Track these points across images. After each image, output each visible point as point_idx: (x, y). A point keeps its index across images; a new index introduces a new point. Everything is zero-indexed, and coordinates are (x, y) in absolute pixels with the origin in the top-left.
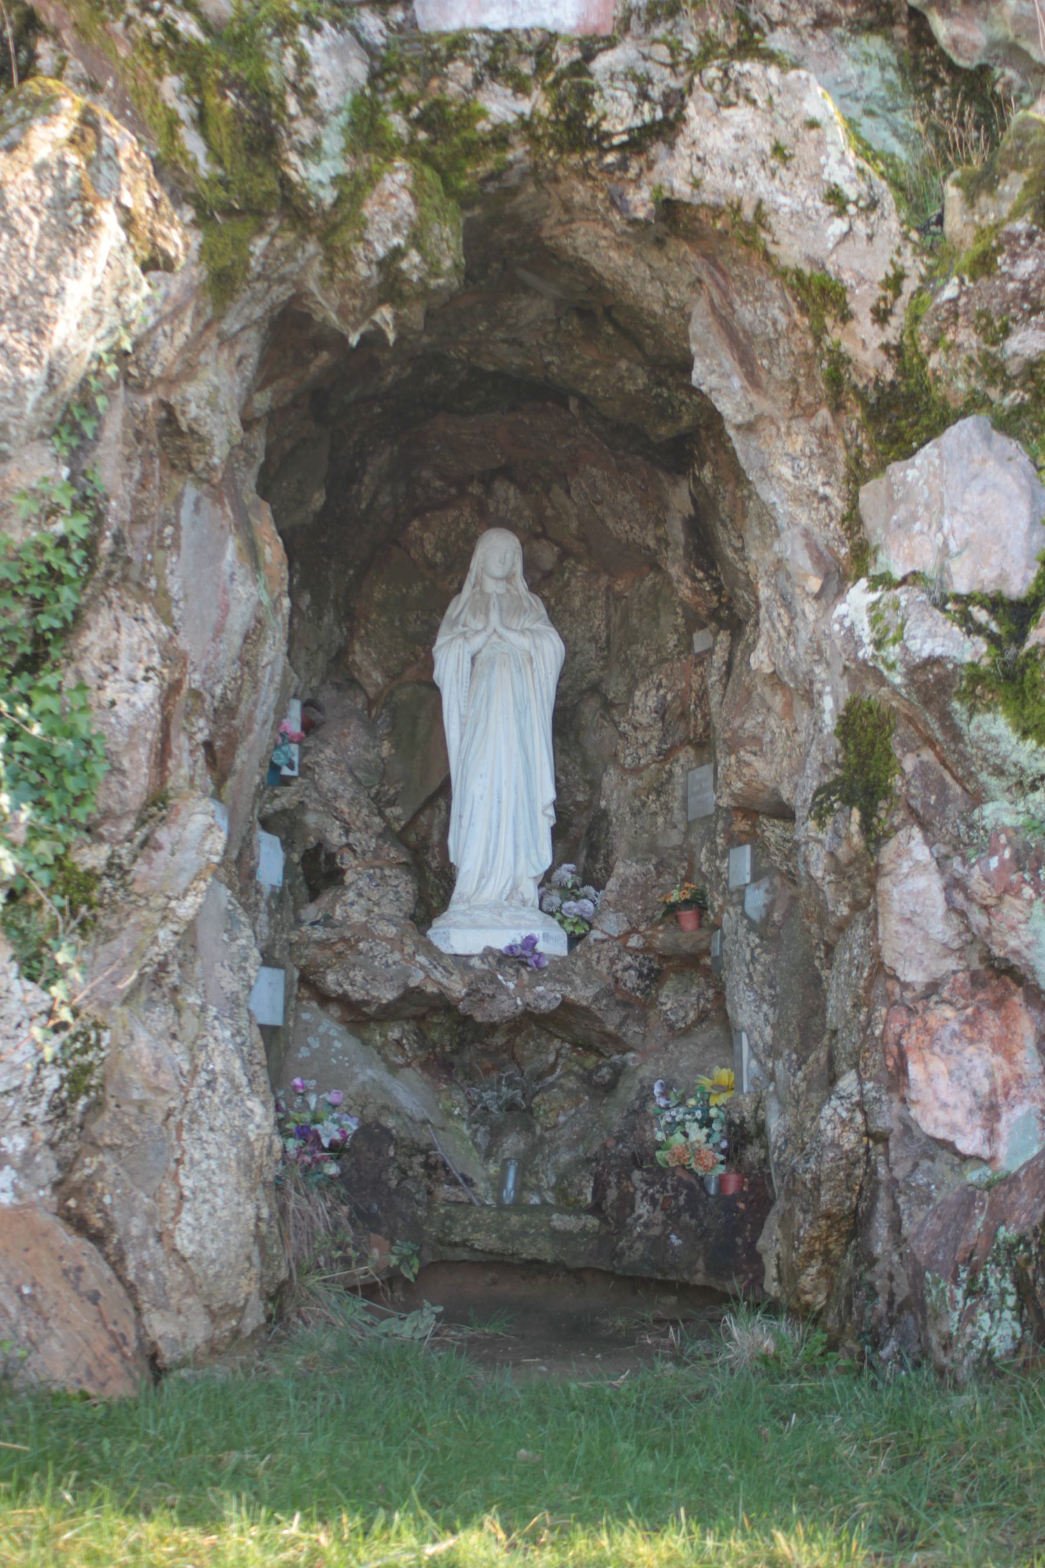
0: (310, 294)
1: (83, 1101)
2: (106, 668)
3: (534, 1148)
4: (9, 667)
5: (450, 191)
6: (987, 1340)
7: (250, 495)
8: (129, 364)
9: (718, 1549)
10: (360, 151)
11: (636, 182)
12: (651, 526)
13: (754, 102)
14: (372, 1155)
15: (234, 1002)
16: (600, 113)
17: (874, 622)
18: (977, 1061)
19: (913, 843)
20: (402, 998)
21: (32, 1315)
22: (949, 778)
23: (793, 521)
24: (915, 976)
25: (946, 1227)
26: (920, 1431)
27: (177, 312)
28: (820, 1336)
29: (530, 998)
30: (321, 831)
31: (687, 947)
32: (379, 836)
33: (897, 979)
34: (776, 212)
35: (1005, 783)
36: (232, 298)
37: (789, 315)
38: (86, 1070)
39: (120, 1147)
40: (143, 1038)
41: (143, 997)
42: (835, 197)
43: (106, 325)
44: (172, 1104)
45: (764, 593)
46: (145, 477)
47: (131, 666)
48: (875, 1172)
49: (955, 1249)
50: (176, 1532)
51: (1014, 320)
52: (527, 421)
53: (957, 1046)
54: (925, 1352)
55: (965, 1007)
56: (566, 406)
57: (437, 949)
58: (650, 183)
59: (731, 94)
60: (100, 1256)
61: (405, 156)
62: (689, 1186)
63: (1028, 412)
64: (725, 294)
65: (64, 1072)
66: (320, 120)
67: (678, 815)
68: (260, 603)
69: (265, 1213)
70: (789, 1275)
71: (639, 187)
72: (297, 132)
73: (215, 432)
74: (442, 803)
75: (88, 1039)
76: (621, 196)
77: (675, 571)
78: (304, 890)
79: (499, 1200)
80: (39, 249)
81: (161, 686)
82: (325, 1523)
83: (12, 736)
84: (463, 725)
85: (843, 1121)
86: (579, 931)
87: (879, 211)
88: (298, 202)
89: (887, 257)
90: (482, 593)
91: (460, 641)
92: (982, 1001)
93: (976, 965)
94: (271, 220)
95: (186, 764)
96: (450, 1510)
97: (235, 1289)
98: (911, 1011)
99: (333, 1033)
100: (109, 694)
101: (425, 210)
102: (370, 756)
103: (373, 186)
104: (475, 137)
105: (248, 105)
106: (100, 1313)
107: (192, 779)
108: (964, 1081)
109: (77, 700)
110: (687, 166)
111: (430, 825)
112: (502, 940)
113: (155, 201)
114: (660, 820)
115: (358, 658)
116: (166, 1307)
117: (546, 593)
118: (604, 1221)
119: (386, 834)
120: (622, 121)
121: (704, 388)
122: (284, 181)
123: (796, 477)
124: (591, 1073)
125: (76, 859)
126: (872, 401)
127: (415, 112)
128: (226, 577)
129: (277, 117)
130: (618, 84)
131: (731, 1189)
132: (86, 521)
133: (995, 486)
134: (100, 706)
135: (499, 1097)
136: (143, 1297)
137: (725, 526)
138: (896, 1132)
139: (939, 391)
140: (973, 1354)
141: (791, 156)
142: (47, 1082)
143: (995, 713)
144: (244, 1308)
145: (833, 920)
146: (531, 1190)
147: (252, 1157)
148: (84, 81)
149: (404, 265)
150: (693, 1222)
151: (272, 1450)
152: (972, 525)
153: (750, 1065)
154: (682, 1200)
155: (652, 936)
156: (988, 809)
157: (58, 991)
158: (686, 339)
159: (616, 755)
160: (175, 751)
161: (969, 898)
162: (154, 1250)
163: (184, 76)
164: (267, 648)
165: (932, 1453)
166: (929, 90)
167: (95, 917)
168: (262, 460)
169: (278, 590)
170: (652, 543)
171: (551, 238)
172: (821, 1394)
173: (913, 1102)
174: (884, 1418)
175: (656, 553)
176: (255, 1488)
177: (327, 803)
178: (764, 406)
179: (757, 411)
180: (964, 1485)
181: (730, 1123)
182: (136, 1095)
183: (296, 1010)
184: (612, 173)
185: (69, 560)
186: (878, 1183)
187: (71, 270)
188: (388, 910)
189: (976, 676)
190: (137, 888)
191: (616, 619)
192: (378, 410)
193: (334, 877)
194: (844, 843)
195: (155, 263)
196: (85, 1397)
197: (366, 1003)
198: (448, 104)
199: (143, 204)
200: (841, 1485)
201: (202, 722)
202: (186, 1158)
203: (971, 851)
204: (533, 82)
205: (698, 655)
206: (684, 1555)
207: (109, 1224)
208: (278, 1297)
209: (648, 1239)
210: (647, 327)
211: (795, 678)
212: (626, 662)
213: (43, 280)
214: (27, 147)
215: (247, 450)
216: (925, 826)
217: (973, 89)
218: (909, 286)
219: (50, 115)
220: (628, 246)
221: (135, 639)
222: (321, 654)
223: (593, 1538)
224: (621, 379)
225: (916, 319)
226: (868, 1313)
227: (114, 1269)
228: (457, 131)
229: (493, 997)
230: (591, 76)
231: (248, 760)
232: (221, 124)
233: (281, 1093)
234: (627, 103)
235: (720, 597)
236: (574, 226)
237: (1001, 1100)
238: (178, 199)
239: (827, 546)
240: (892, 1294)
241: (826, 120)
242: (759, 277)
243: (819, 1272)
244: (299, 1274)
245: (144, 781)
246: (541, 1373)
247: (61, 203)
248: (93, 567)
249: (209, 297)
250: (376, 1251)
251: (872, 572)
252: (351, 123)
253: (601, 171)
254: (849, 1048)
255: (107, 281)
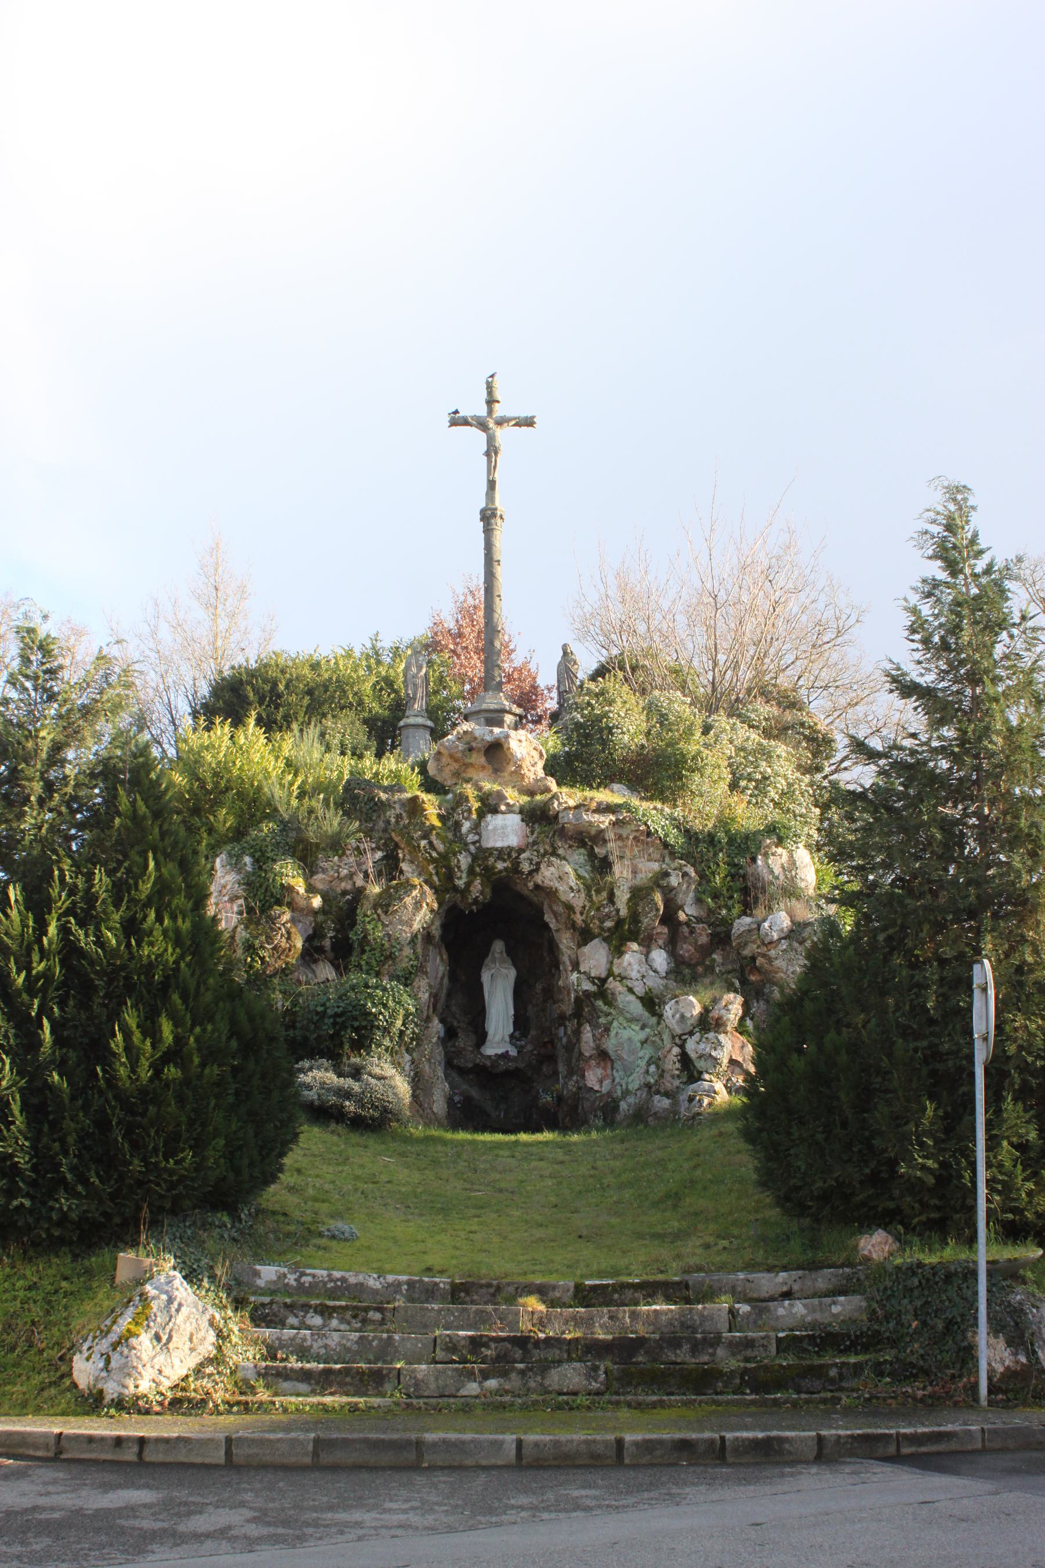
59: (550, 864)
112: (500, 1051)
247: (416, 903)
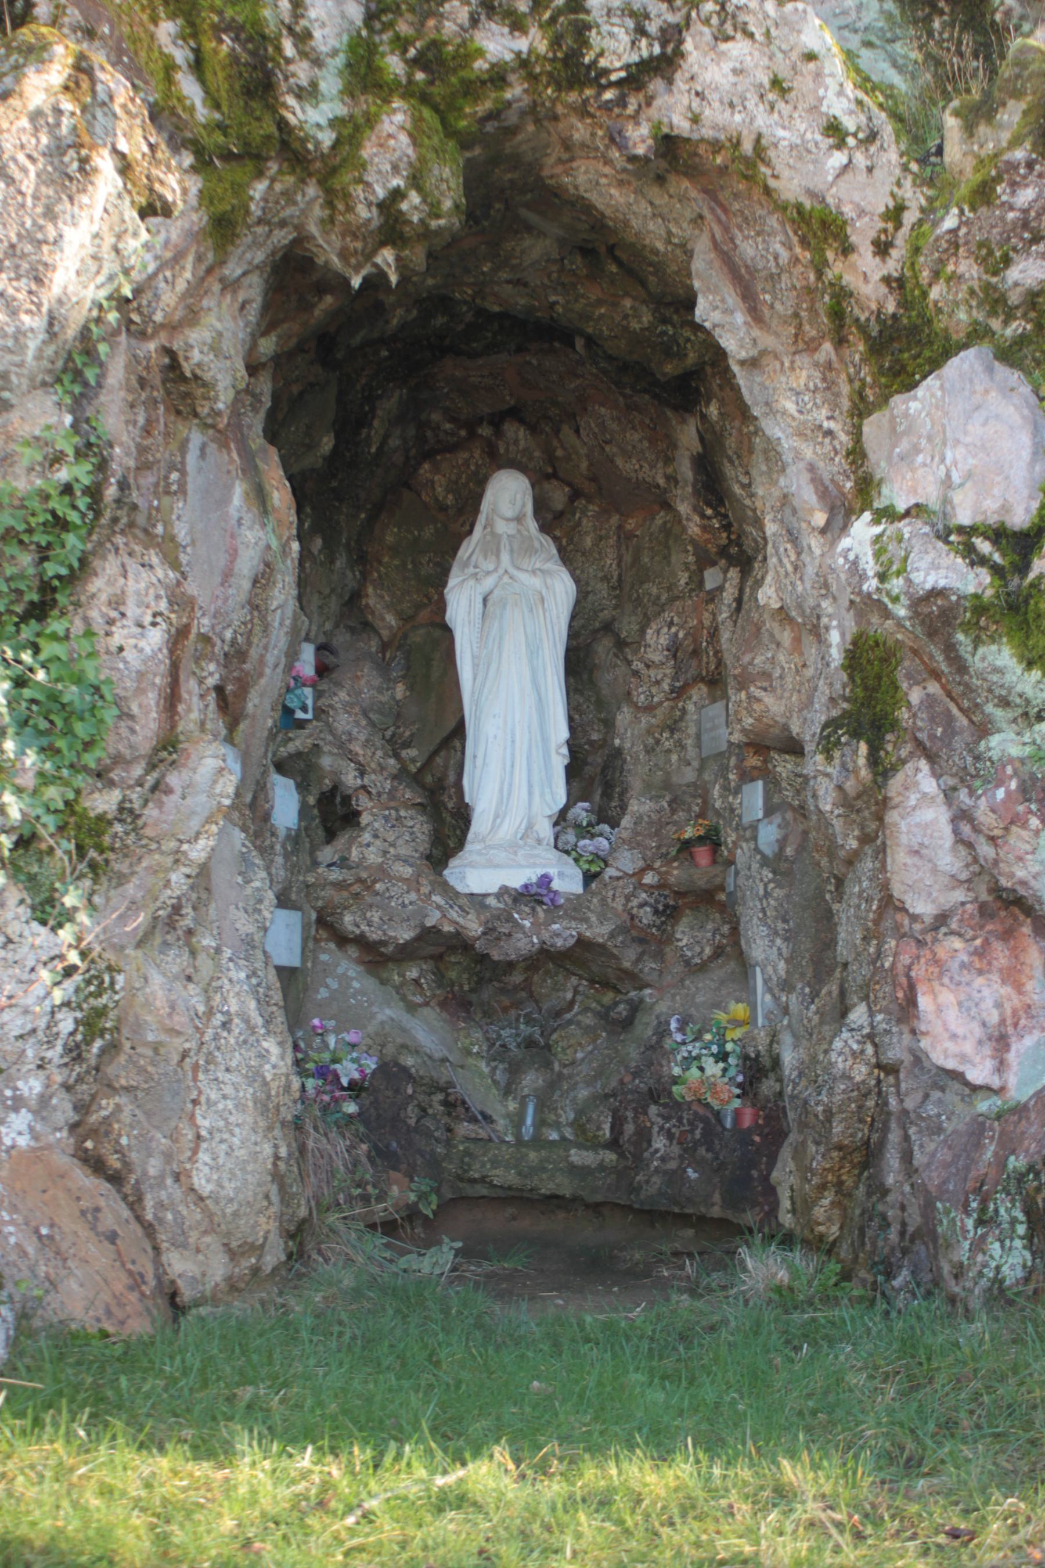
0: (311, 238)
1: (98, 1044)
2: (114, 614)
3: (552, 1086)
4: (17, 615)
5: (449, 132)
6: (998, 1268)
7: (257, 440)
8: (130, 308)
9: (725, 1477)
10: (357, 93)
11: (635, 118)
12: (660, 465)
13: (751, 36)
14: (389, 1093)
15: (249, 943)
16: (598, 50)
17: (877, 555)
18: (986, 992)
19: (920, 776)
20: (418, 938)
21: (51, 1255)
22: (955, 710)
23: (798, 456)
24: (923, 907)
25: (956, 1157)
26: (929, 1359)
27: (178, 257)
28: (834, 1267)
29: (546, 936)
30: (336, 773)
31: (702, 883)
32: (394, 777)
33: (906, 911)
34: (776, 145)
35: (1010, 714)
36: (233, 243)
37: (791, 249)
38: (101, 1013)
39: (136, 1088)
40: (157, 980)
41: (158, 940)
42: (834, 130)
43: (105, 272)
44: (187, 1045)
45: (771, 528)
46: (149, 422)
47: (139, 611)
48: (886, 1103)
49: (965, 1180)
50: (190, 1465)
51: (1015, 249)
52: (535, 362)
53: (966, 977)
54: (936, 1282)
55: (974, 939)
56: (572, 346)
57: (453, 888)
58: (649, 120)
60: (118, 1197)
61: (403, 97)
62: (705, 1120)
63: (1030, 342)
64: (726, 229)
65: (79, 1015)
66: (317, 62)
67: (691, 753)
68: (268, 547)
69: (283, 1152)
70: (802, 1207)
71: (638, 124)
72: (294, 75)
73: (219, 377)
74: (457, 743)
75: (102, 982)
76: (620, 132)
77: (684, 508)
78: (321, 833)
79: (518, 1137)
80: (36, 197)
81: (169, 631)
82: (337, 1456)
83: (20, 683)
84: (475, 666)
85: (854, 1053)
86: (594, 869)
87: (878, 143)
88: (296, 145)
89: (887, 189)
90: (493, 534)
91: (472, 582)
92: (990, 932)
93: (984, 897)
94: (270, 164)
95: (196, 708)
96: (461, 1442)
97: (253, 1227)
98: (920, 943)
99: (351, 973)
100: (116, 640)
101: (423, 151)
102: (385, 698)
103: (372, 128)
104: (473, 77)
105: (245, 49)
106: (119, 1253)
107: (202, 724)
108: (974, 1011)
109: (85, 646)
110: (685, 102)
111: (446, 767)
112: (516, 879)
113: (151, 146)
114: (674, 757)
115: (371, 602)
116: (185, 1246)
117: (558, 533)
118: (622, 1155)
119: (402, 775)
120: (620, 57)
121: (707, 325)
122: (282, 124)
123: (800, 412)
124: (609, 1009)
125: (87, 804)
126: (874, 334)
127: (412, 52)
128: (234, 522)
129: (273, 60)
130: (615, 20)
131: (747, 1122)
132: (90, 467)
133: (997, 417)
134: (108, 652)
135: (518, 1035)
136: (162, 1237)
137: (731, 462)
138: (906, 1063)
139: (941, 323)
140: (984, 1283)
141: (790, 89)
142: (61, 1025)
143: (1000, 644)
144: (263, 1246)
145: (842, 853)
146: (550, 1126)
147: (269, 1097)
148: (80, 28)
149: (404, 206)
150: (710, 1156)
151: (285, 1384)
152: (974, 456)
153: (764, 999)
154: (698, 1134)
155: (667, 873)
156: (995, 740)
157: (66, 934)
158: (689, 275)
159: (629, 693)
160: (185, 696)
161: (976, 830)
162: (172, 1190)
163: (180, 21)
164: (276, 592)
165: (941, 1379)
166: (928, 20)
167: (107, 862)
168: (269, 404)
169: (286, 534)
170: (661, 481)
171: (552, 177)
172: (833, 1324)
173: (923, 1033)
174: (895, 1346)
175: (665, 491)
176: (269, 1423)
177: (341, 746)
178: (768, 341)
179: (761, 346)
180: (972, 1412)
181: (746, 1057)
182: (151, 1037)
183: (314, 951)
184: (611, 110)
185: (74, 507)
186: (889, 1114)
187: (68, 217)
188: (404, 851)
189: (980, 608)
190: (148, 832)
191: (628, 558)
192: (385, 353)
193: (351, 818)
194: (852, 776)
195: (153, 209)
196: (105, 1335)
197: (383, 943)
198: (445, 43)
199: (139, 150)
200: (848, 1413)
201: (212, 667)
202: (203, 1099)
203: (978, 783)
204: (530, 20)
205: (709, 592)
206: (691, 1483)
207: (127, 1164)
208: (299, 1236)
209: (665, 1172)
210: (651, 264)
211: (803, 614)
212: (638, 601)
213: (41, 228)
214: (21, 95)
215: (254, 395)
216: (932, 758)
217: (973, 18)
218: (910, 217)
219: (43, 62)
220: (629, 183)
221: (143, 585)
222: (334, 598)
223: (602, 1468)
224: (626, 317)
225: (917, 250)
226: (880, 1244)
227: (132, 1209)
228: (455, 71)
229: (510, 935)
230: (588, 12)
231: (260, 704)
232: (218, 68)
233: (300, 1034)
234: (625, 39)
235: (730, 533)
236: (575, 165)
237: (1010, 1030)
238: (176, 145)
239: (832, 480)
240: (904, 1224)
241: (823, 51)
242: (760, 212)
243: (832, 1203)
244: (319, 1211)
245: (153, 726)
246: (557, 1306)
247: (58, 150)
248: (98, 514)
249: (210, 242)
250: (395, 1188)
251: (876, 505)
252: (349, 65)
253: (599, 108)
254: (859, 980)
255: (105, 228)
